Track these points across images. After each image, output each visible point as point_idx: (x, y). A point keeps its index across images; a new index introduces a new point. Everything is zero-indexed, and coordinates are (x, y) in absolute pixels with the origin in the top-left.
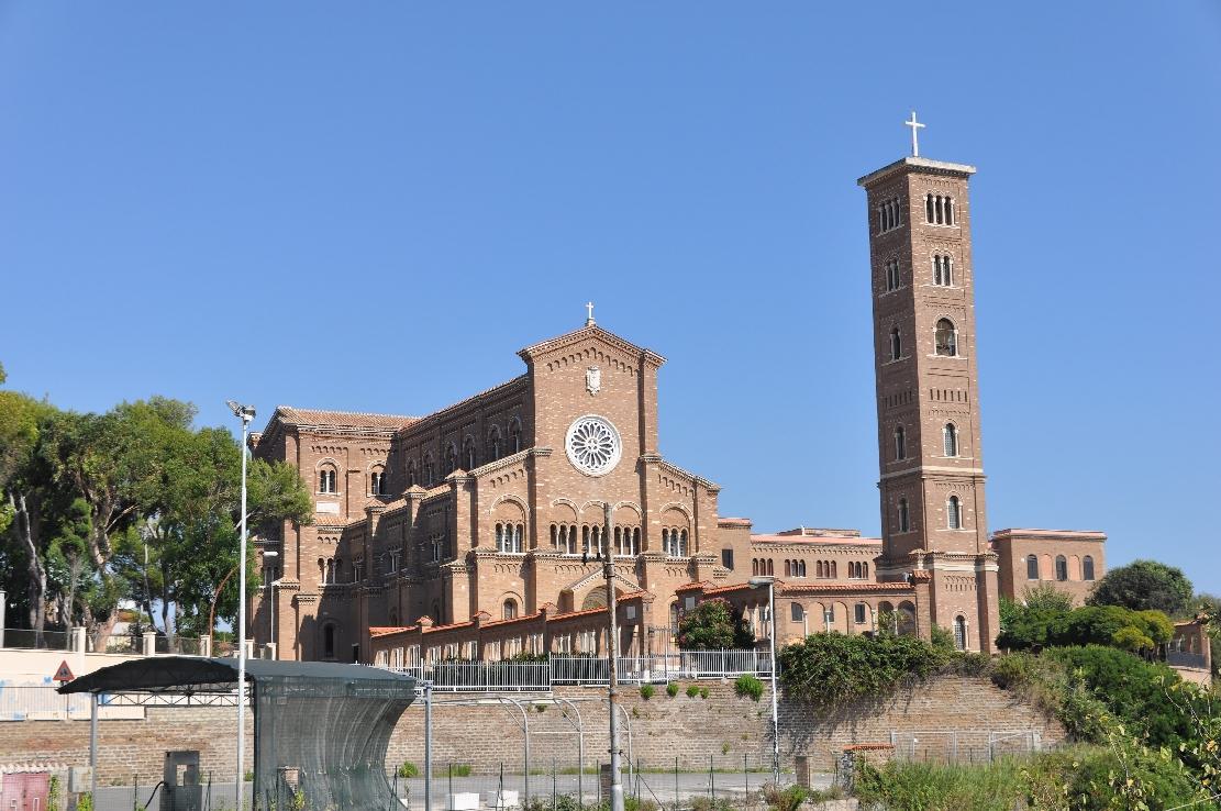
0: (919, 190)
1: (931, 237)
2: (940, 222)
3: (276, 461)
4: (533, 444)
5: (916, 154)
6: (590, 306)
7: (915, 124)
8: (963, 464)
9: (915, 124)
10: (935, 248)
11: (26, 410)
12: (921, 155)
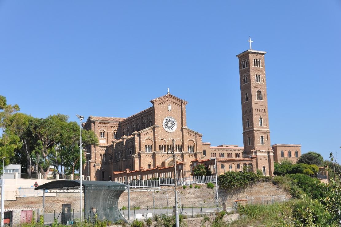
0: (252, 58)
7: (250, 41)
8: (264, 128)
9: (250, 41)
10: (256, 73)
12: (252, 49)
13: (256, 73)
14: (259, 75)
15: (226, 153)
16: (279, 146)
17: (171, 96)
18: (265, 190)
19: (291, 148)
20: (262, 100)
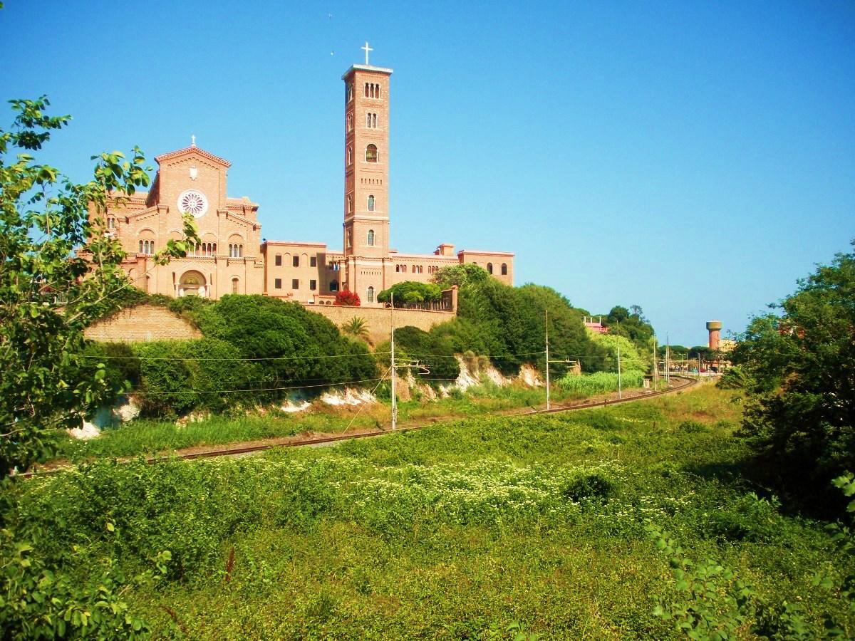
0: (360, 80)
1: (366, 104)
2: (373, 97)
3: (784, 406)
4: (158, 202)
5: (367, 63)
6: (193, 137)
7: (367, 49)
8: (379, 215)
9: (367, 49)
10: (369, 110)
11: (105, 244)
12: (370, 63)
13: (369, 110)
14: (375, 115)
15: (410, 265)
16: (469, 254)
17: (193, 151)
18: (151, 321)
19: (494, 258)
20: (378, 163)
